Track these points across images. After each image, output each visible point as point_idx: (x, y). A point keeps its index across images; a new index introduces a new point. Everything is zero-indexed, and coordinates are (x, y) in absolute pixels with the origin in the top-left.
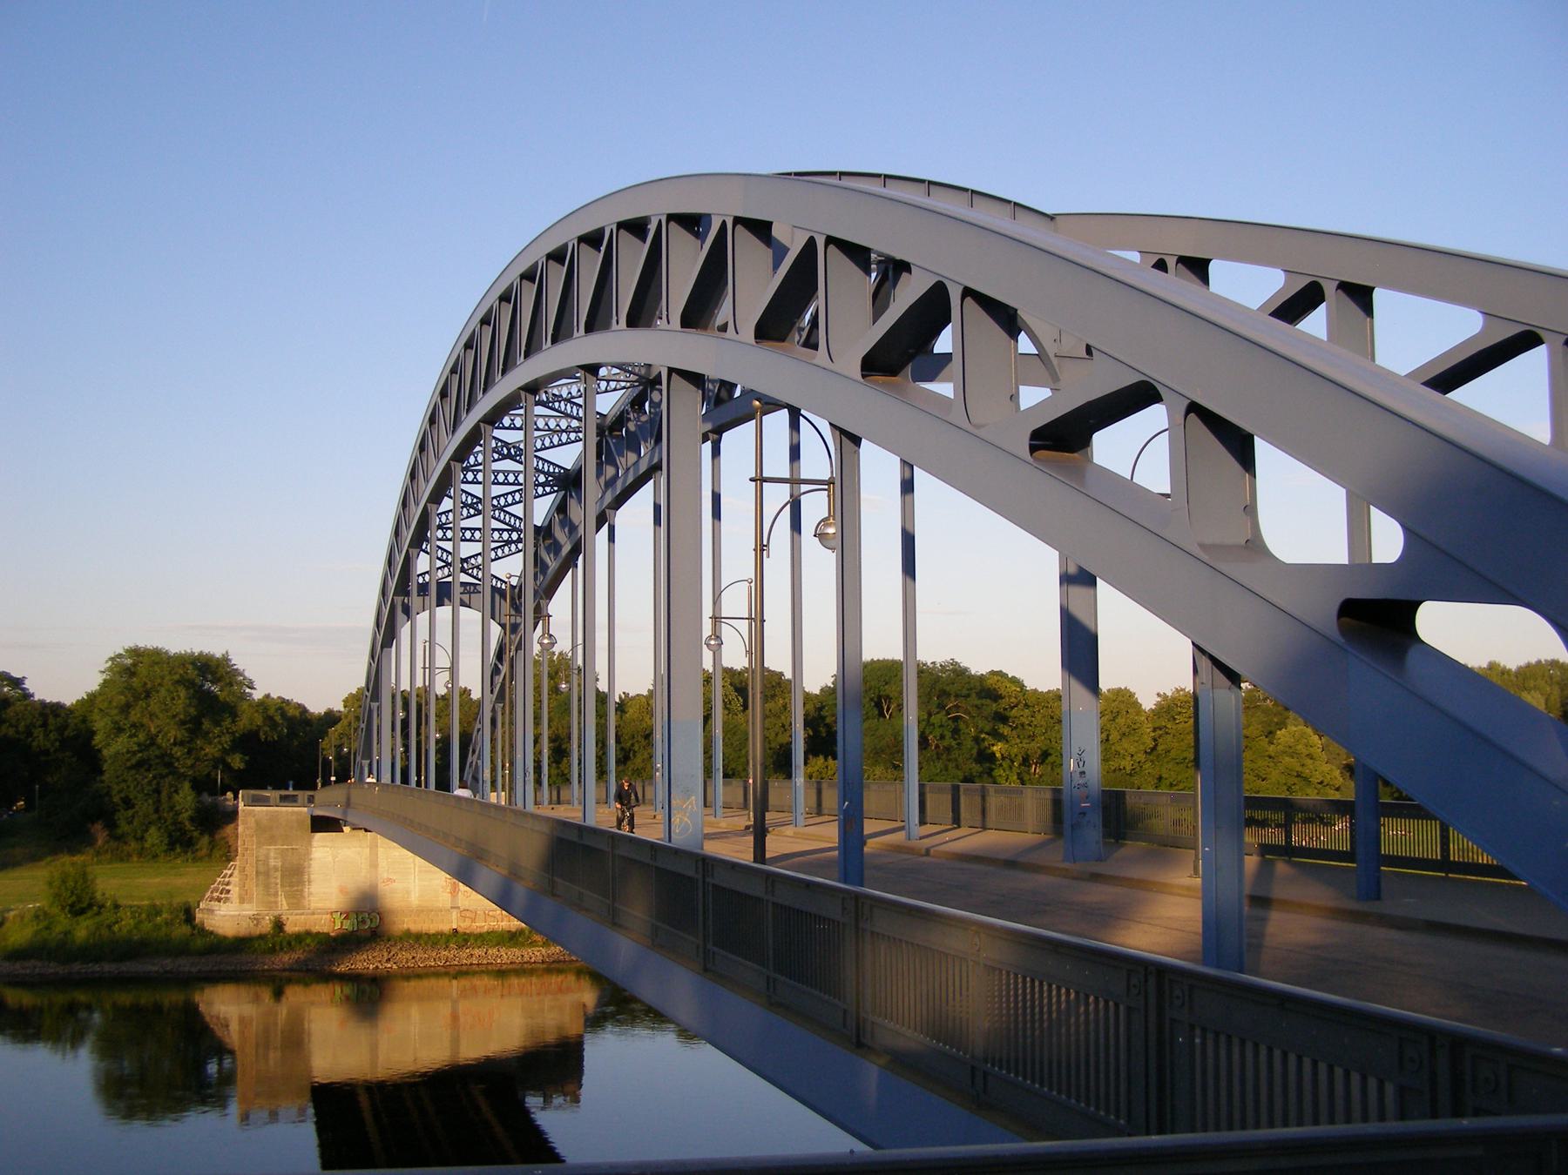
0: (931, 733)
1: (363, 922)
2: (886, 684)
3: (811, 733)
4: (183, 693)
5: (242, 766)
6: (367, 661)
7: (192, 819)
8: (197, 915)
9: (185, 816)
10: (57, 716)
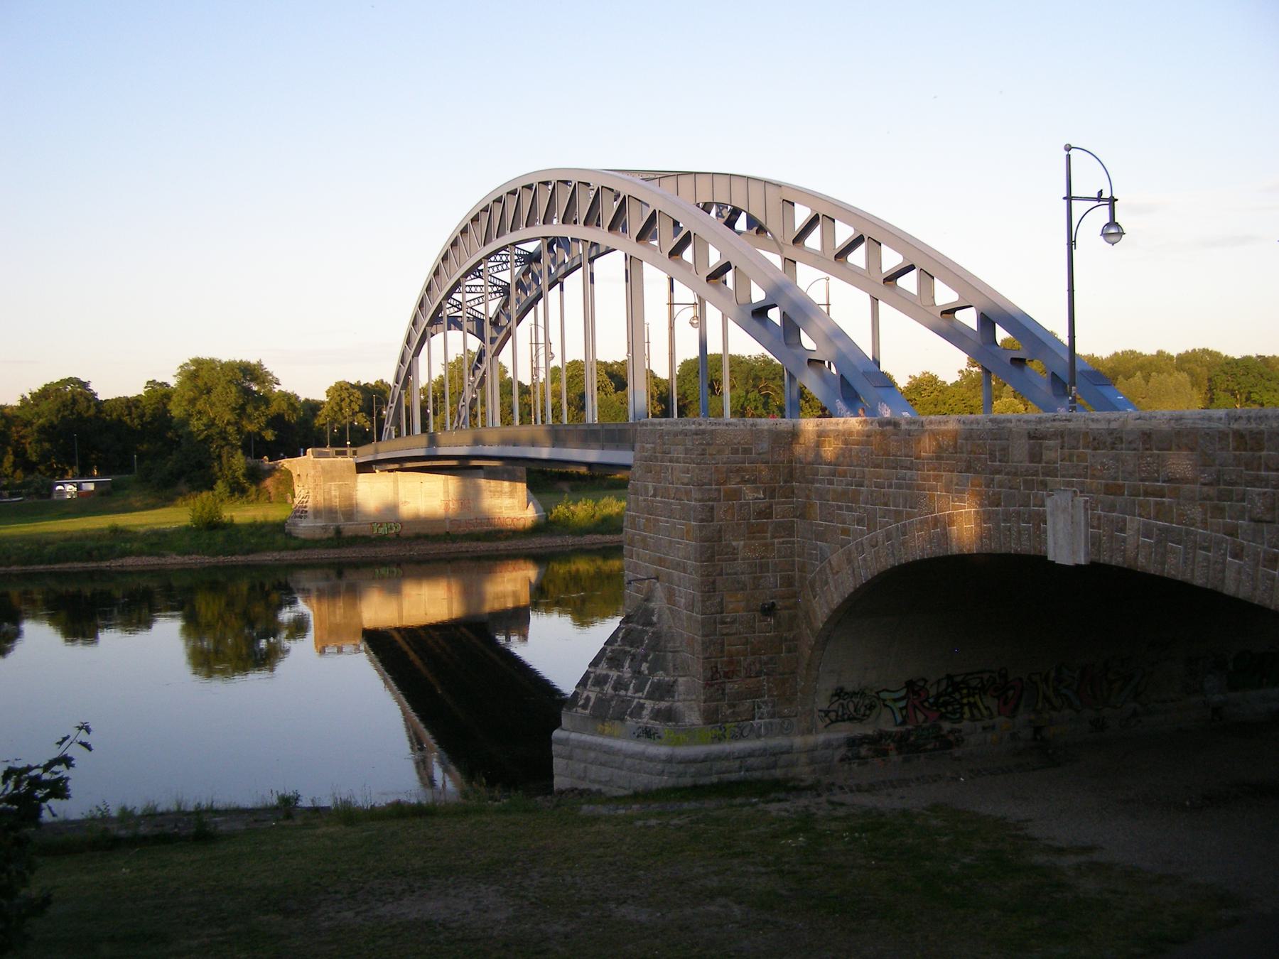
0: (748, 405)
1: (391, 529)
2: (717, 371)
3: (664, 407)
4: (234, 389)
5: (273, 438)
6: (396, 364)
7: (244, 475)
8: (286, 527)
9: (239, 473)
10: (137, 407)
